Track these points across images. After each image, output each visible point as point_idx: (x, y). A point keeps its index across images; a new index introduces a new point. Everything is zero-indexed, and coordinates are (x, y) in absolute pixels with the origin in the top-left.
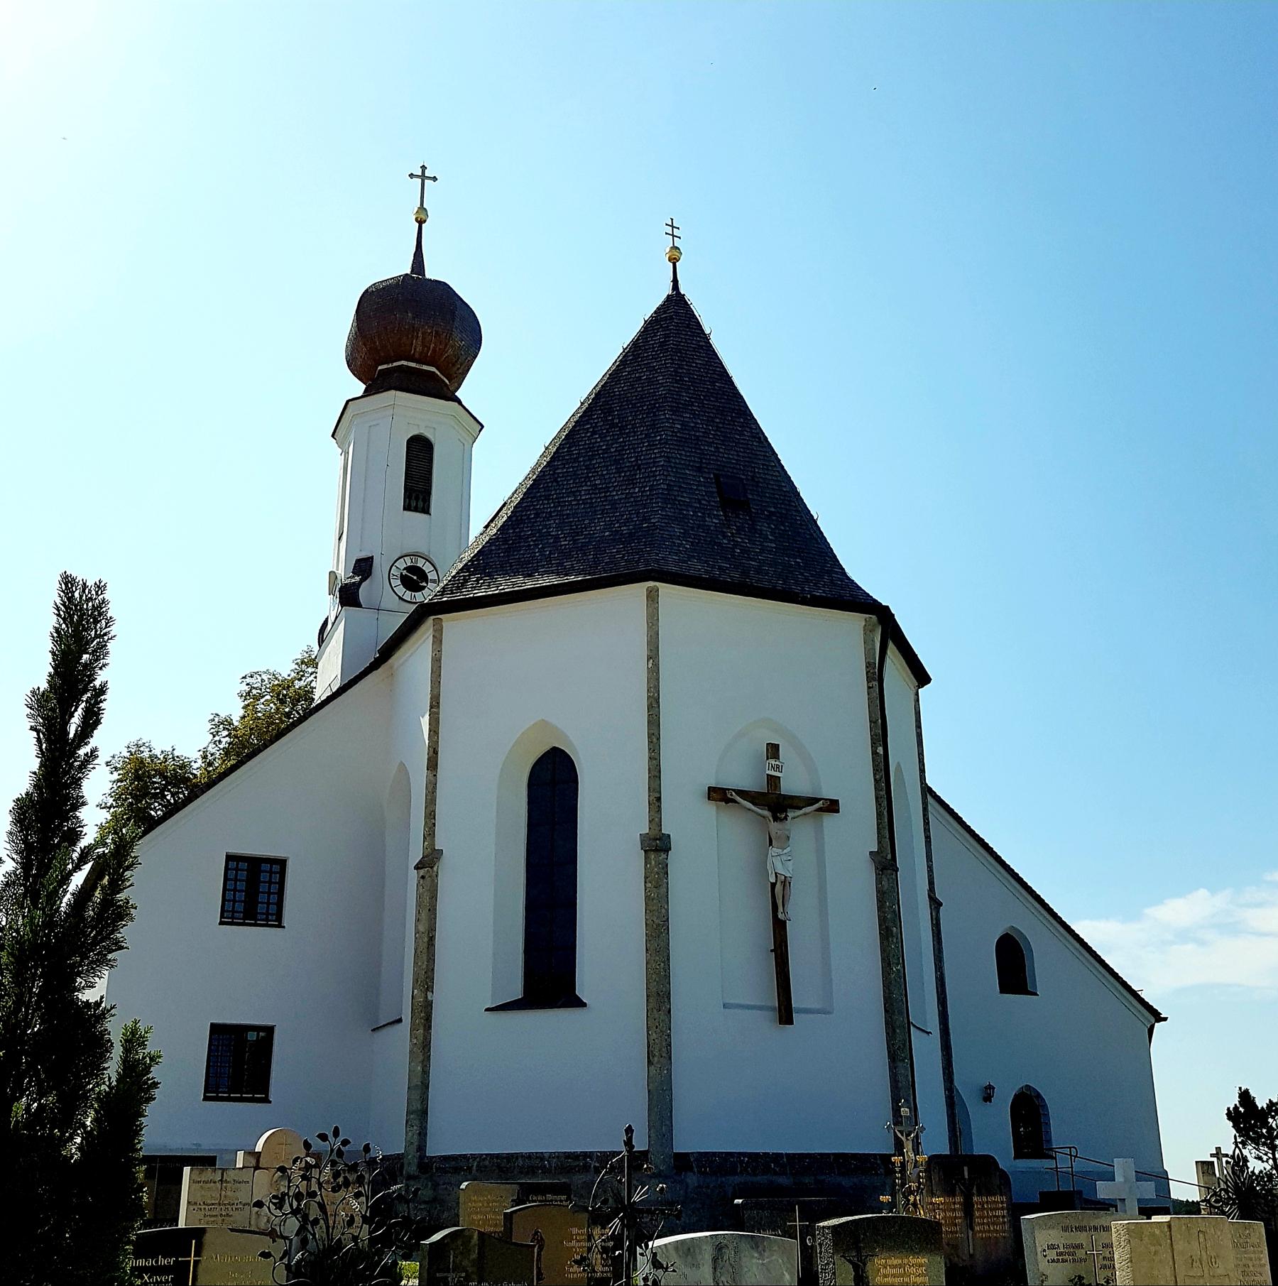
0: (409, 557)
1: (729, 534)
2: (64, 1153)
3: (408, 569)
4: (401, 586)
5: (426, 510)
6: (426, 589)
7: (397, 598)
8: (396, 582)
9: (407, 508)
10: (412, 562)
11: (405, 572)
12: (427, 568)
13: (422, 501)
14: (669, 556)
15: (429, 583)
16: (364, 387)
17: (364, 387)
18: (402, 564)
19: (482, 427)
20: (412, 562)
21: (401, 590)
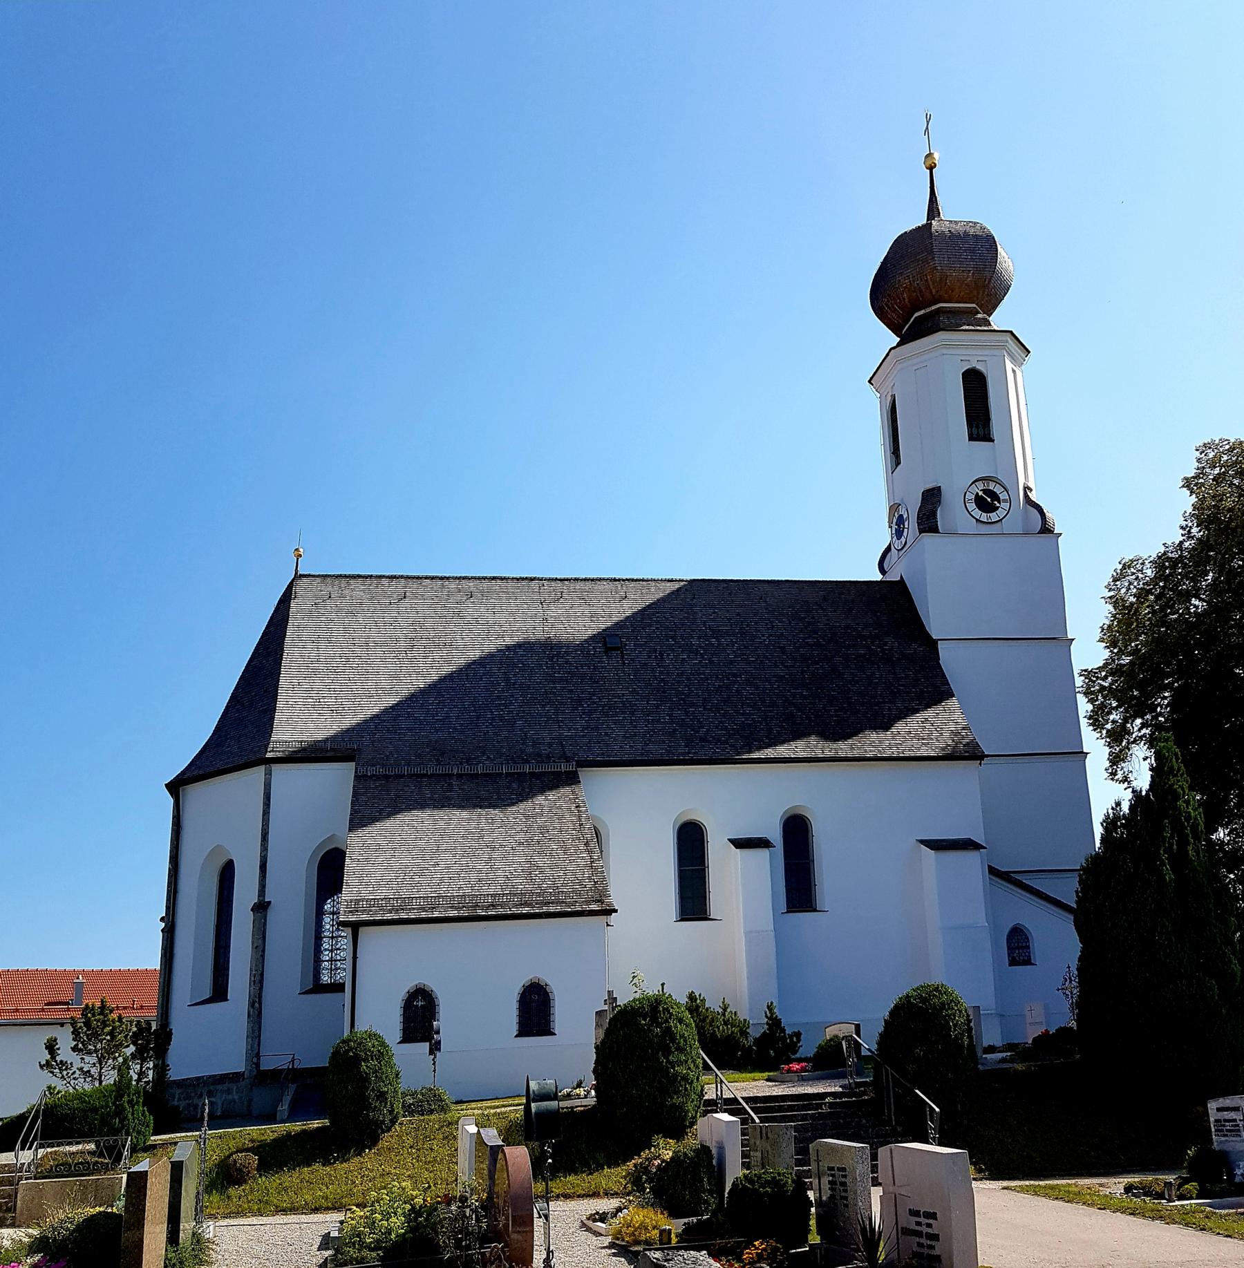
0: (981, 482)
1: (1113, 859)
2: (150, 1090)
3: (995, 509)
4: (977, 509)
5: (988, 438)
6: (1000, 508)
7: (975, 520)
8: (972, 506)
9: (971, 438)
10: (984, 485)
11: (981, 493)
12: (998, 490)
13: (976, 427)
14: (438, 881)
15: (1002, 503)
16: (898, 339)
17: (898, 339)
18: (1001, 513)
19: (1029, 352)
20: (984, 485)
21: (977, 513)
